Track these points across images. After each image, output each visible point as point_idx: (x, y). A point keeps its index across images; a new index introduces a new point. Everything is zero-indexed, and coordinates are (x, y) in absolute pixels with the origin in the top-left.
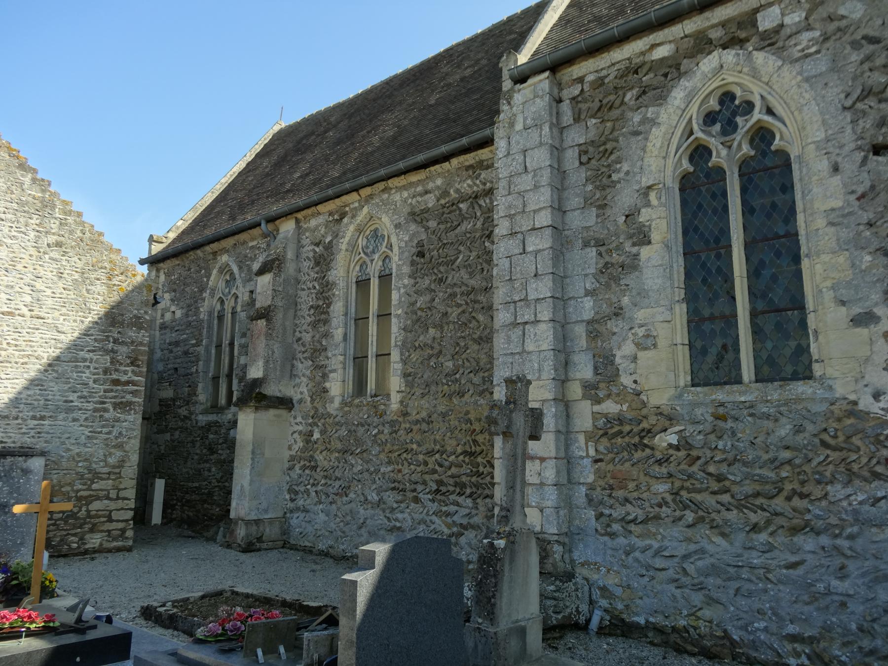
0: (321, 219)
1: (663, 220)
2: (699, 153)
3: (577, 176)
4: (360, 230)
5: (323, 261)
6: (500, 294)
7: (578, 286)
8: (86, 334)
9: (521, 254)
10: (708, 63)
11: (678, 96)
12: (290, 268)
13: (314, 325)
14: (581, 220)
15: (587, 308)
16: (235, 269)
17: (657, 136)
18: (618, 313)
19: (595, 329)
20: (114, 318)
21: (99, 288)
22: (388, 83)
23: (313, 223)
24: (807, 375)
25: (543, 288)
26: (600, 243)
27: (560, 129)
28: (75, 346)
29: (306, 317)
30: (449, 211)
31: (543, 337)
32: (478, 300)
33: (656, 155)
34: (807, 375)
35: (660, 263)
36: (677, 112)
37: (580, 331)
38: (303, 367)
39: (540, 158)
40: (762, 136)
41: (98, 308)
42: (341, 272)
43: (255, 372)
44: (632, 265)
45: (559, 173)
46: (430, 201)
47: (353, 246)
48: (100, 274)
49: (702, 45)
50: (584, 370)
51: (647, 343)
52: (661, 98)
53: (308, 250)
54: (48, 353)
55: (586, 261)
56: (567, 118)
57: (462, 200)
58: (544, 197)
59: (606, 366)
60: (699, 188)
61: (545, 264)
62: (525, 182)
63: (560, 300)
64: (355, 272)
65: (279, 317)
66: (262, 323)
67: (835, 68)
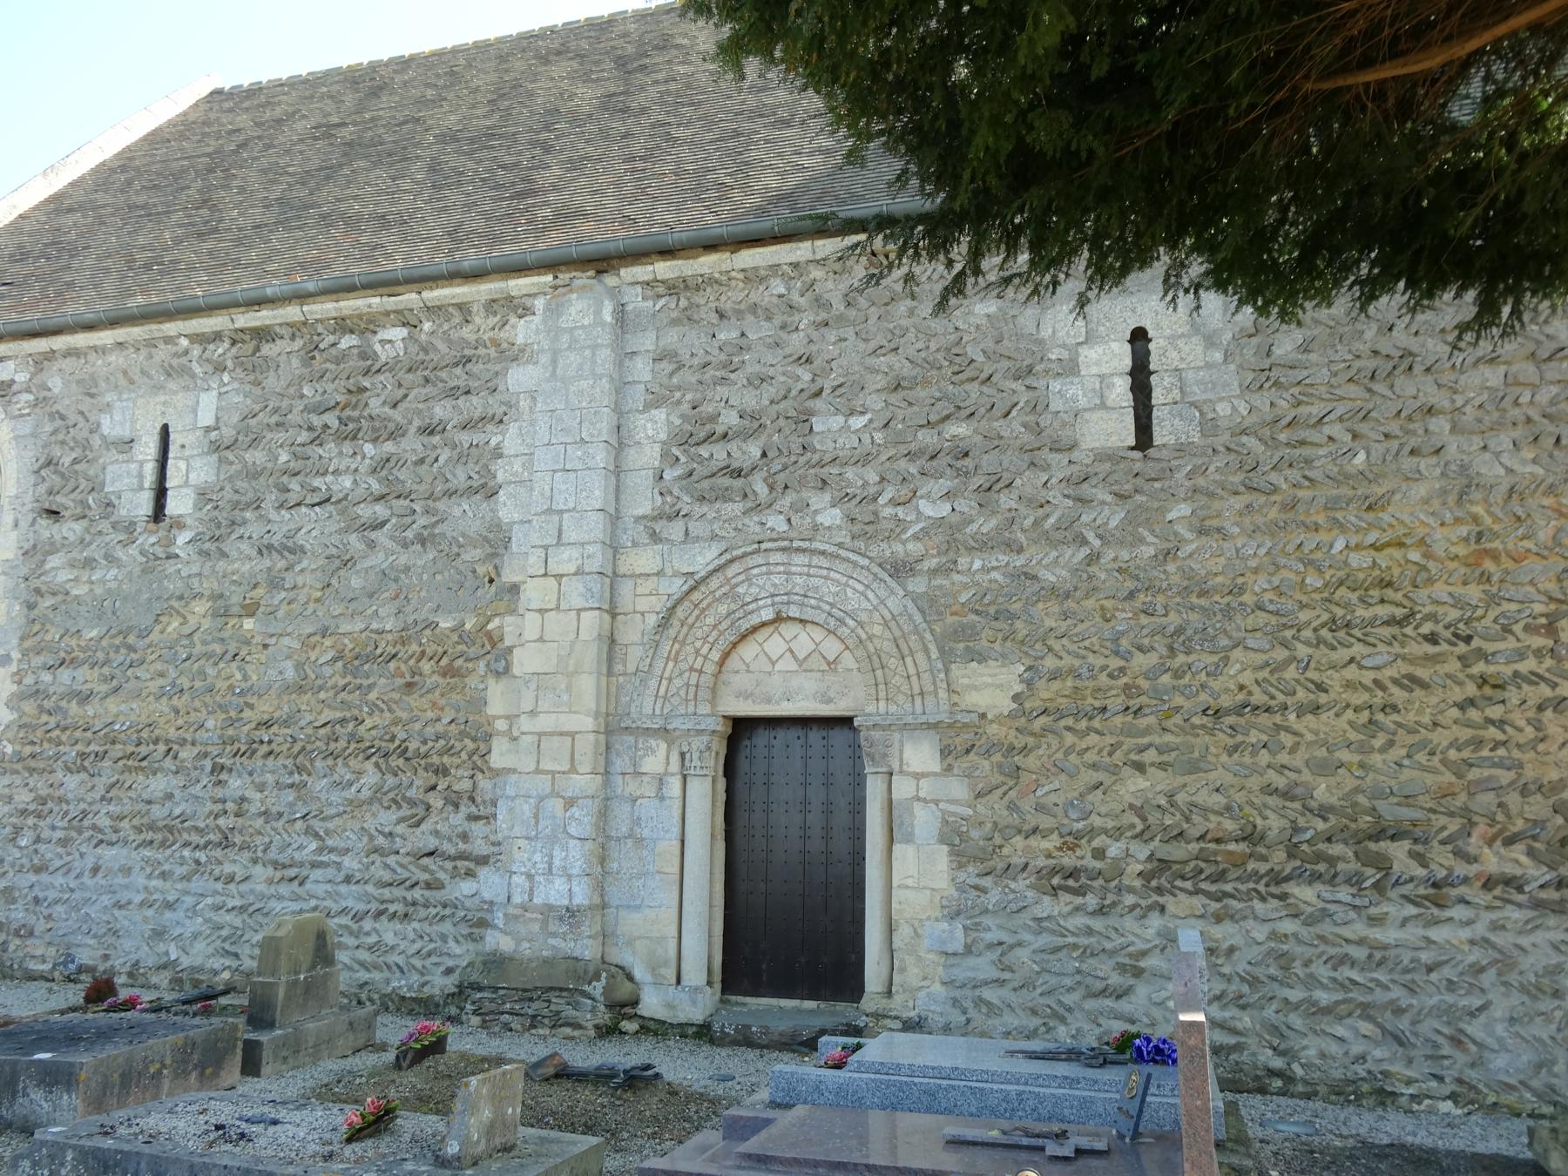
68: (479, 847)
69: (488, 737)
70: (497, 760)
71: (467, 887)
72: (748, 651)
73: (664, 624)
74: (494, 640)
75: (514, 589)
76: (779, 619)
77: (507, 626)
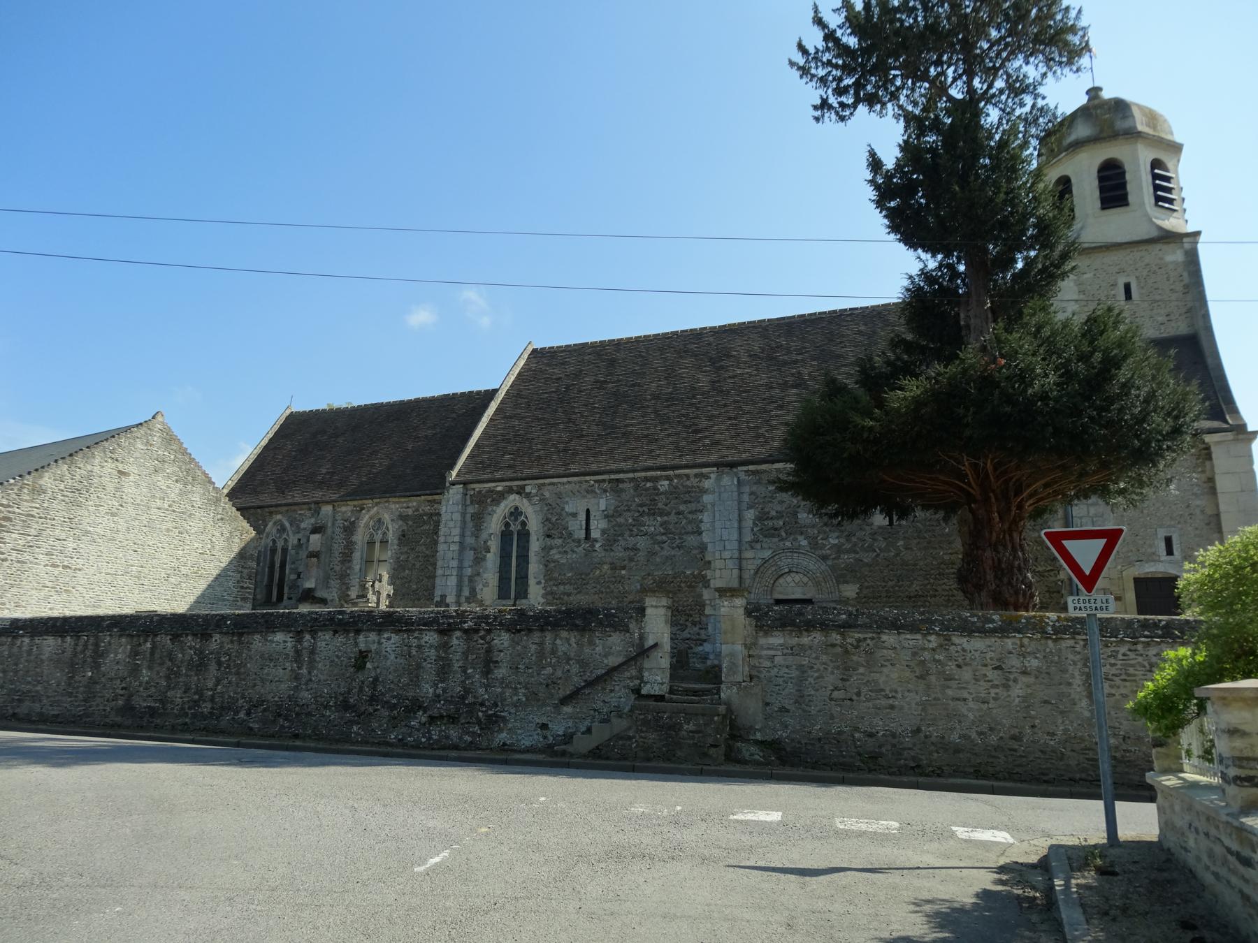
0: (349, 508)
1: (494, 545)
2: (507, 525)
3: (470, 524)
4: (371, 518)
5: (350, 529)
6: (439, 563)
7: (467, 563)
8: (231, 563)
9: (447, 550)
10: (513, 497)
11: (502, 505)
12: (329, 531)
13: (343, 562)
14: (470, 540)
15: (469, 571)
16: (287, 525)
17: (495, 518)
18: (478, 574)
19: (471, 579)
20: (242, 555)
21: (237, 540)
22: (378, 407)
23: (344, 509)
24: (526, 597)
25: (454, 564)
26: (475, 550)
27: (465, 506)
28: (226, 569)
29: (337, 558)
30: (418, 519)
31: (453, 581)
32: (430, 561)
33: (494, 523)
34: (526, 597)
35: (492, 559)
36: (502, 509)
37: (466, 579)
38: (335, 583)
39: (457, 516)
40: (524, 524)
41: (236, 550)
42: (360, 537)
43: (310, 584)
44: (484, 559)
45: (464, 522)
46: (410, 512)
47: (367, 525)
48: (238, 533)
49: (510, 490)
50: (466, 593)
51: (486, 585)
52: (498, 504)
53: (340, 522)
54: (216, 572)
55: (470, 555)
56: (468, 502)
57: (426, 514)
58: (457, 531)
59: (473, 592)
60: (506, 535)
61: (456, 555)
62: (451, 524)
63: (460, 568)
64: (367, 538)
65: (322, 557)
66: (314, 560)
67: (541, 511)
68: (703, 637)
69: (704, 606)
70: (707, 612)
71: (701, 648)
72: (781, 581)
73: (756, 573)
74: (704, 577)
75: (709, 562)
76: (790, 571)
77: (709, 573)
